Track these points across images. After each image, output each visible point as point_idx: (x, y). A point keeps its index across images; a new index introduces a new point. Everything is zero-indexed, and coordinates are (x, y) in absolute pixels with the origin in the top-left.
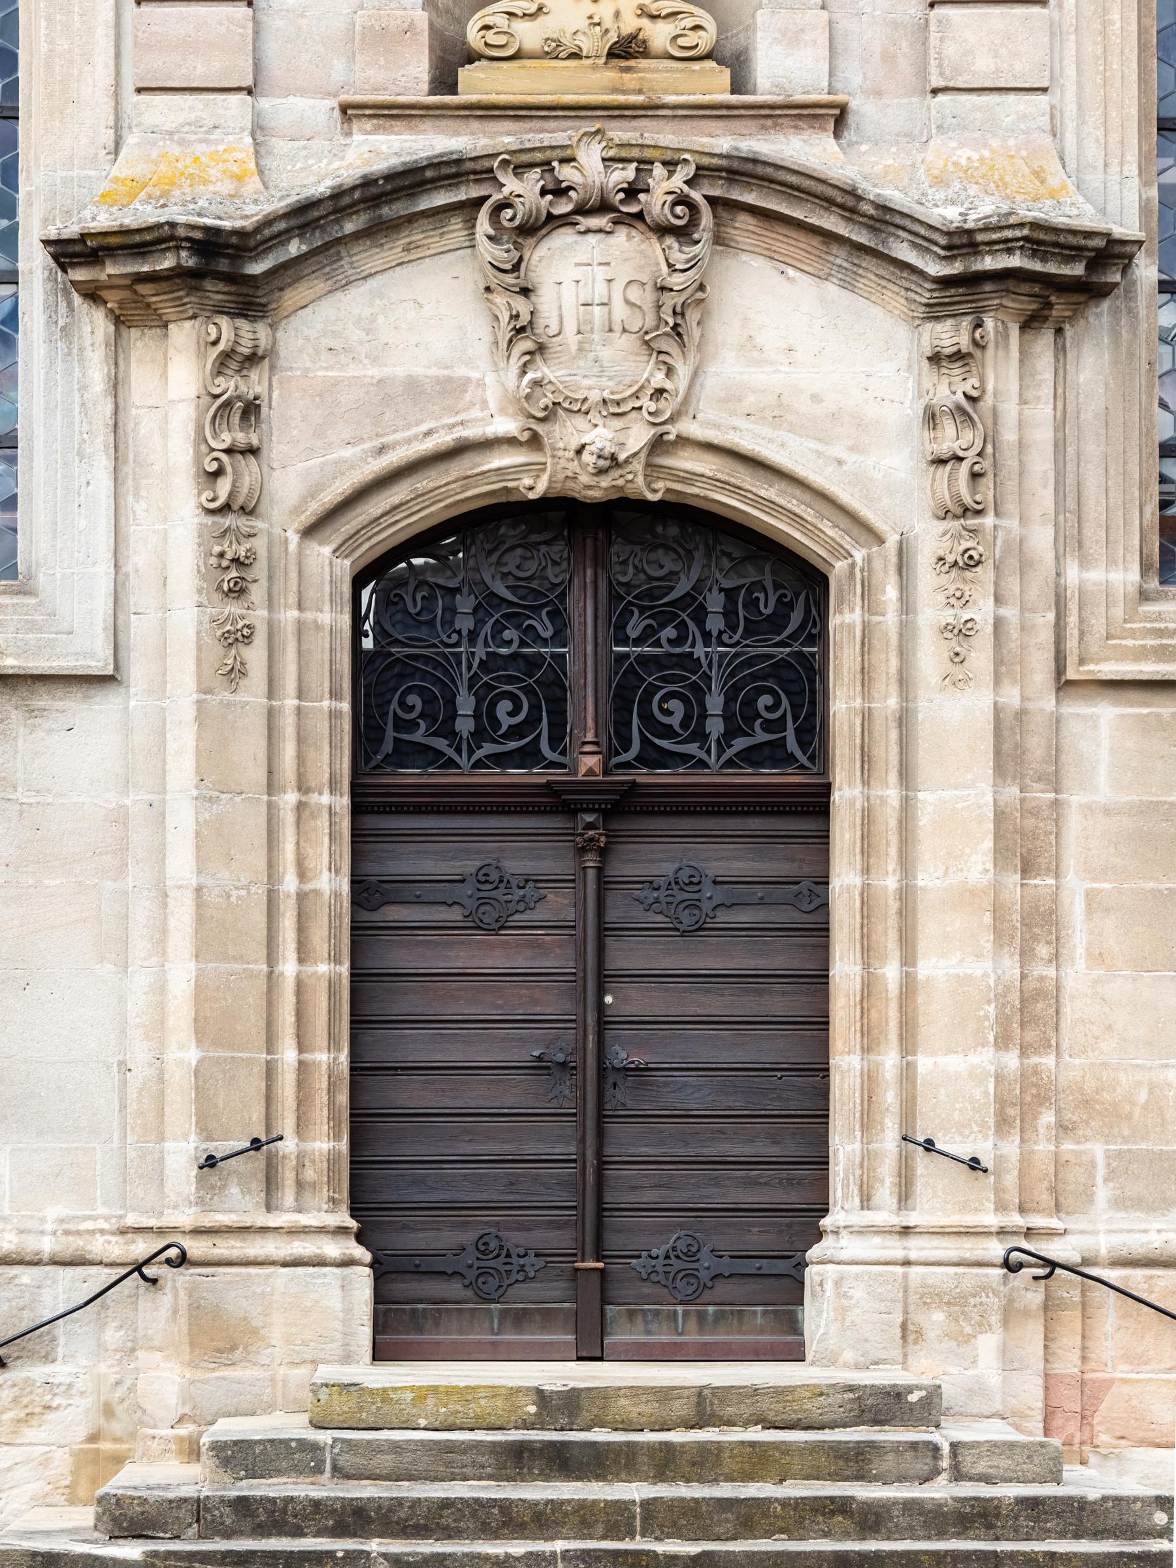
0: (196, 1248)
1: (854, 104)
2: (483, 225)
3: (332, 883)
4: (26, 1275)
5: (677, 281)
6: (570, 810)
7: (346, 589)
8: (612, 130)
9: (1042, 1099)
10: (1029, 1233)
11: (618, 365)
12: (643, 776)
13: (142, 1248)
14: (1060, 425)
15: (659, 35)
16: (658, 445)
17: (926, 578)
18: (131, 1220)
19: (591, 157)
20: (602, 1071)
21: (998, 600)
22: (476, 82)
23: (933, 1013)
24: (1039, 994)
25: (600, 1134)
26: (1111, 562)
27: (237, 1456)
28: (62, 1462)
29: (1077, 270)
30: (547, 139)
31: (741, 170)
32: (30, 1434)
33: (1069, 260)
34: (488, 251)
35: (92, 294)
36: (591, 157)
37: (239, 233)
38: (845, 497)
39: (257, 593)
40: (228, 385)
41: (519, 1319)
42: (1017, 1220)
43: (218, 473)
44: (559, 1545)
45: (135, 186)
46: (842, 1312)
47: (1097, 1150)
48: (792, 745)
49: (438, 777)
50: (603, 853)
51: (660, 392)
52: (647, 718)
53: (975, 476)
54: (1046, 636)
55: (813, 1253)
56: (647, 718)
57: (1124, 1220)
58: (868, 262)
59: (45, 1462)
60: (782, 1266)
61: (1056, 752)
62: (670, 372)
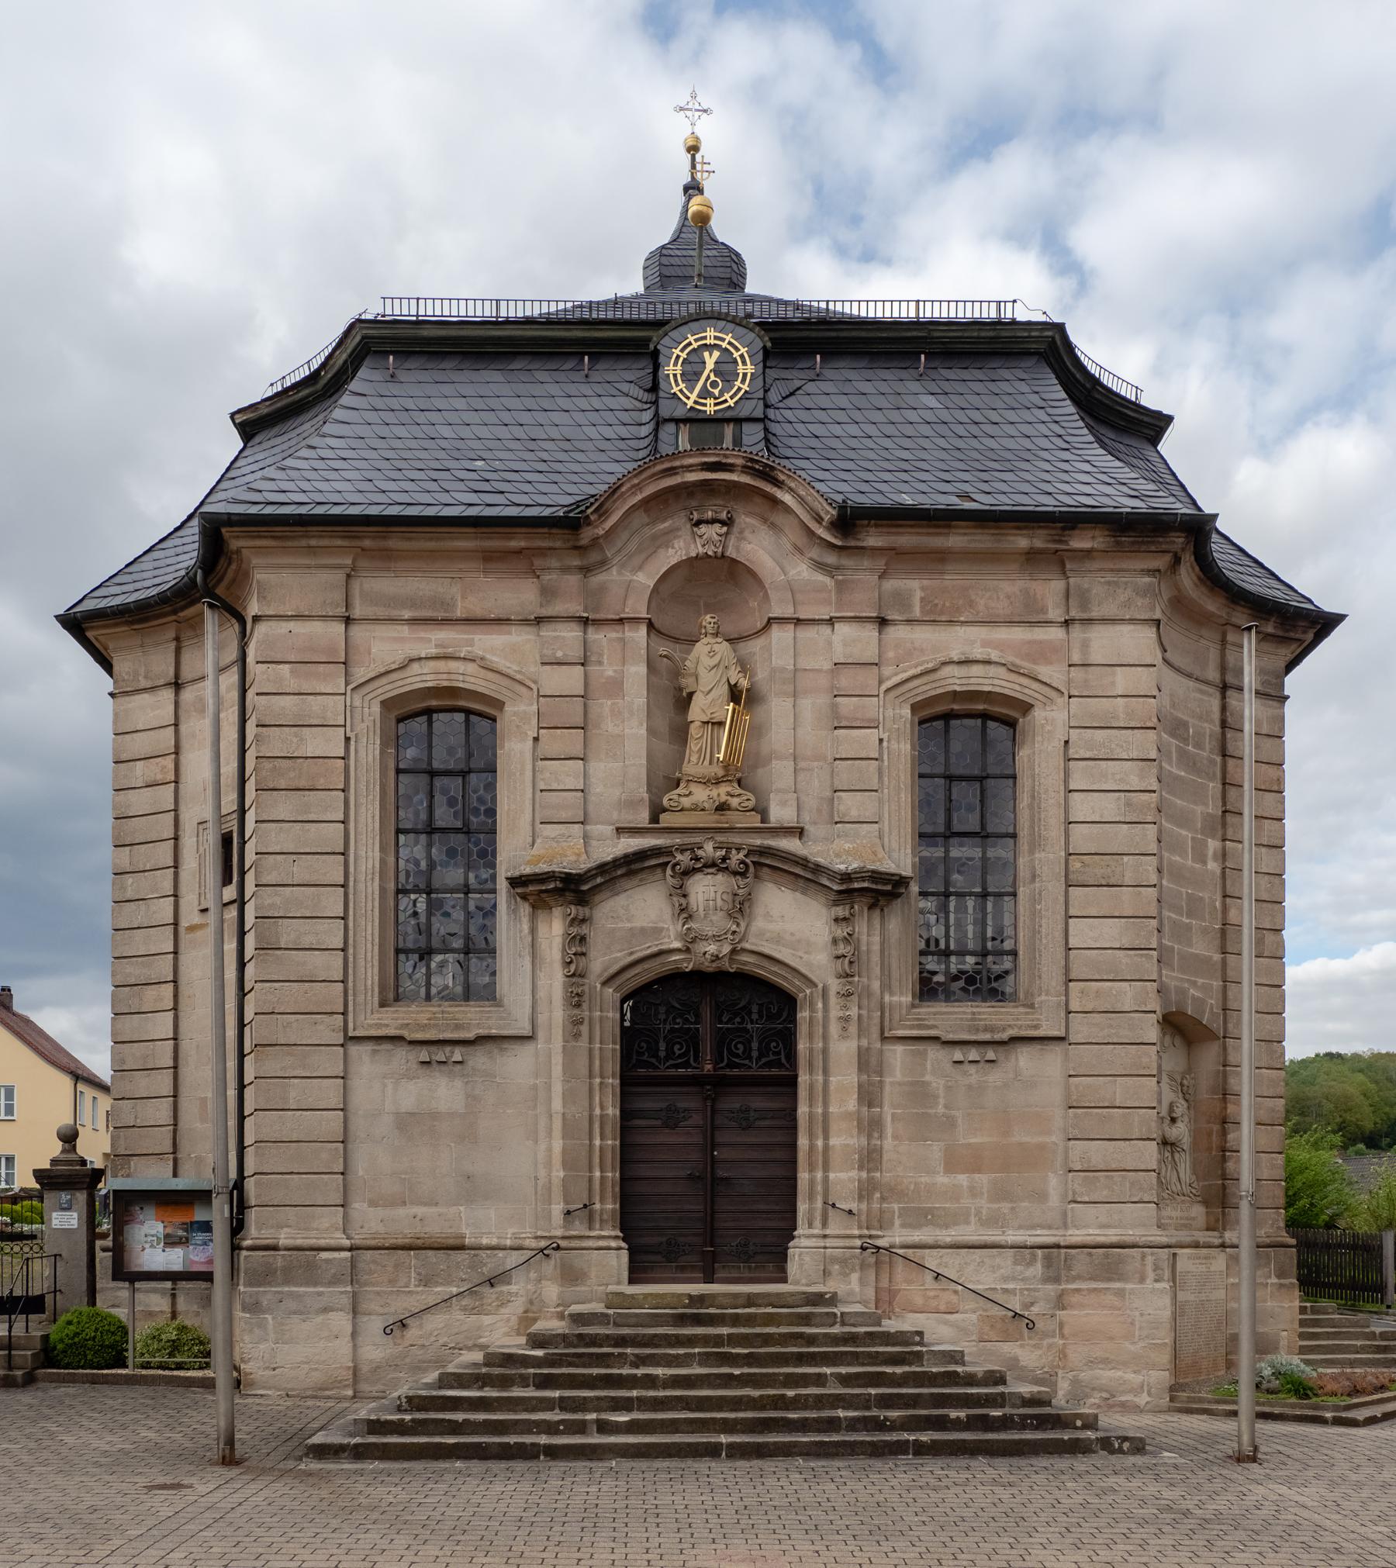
2: (669, 872)
3: (613, 1111)
4: (501, 1254)
8: (92, 628)
9: (875, 1189)
10: (870, 1237)
12: (728, 1072)
13: (543, 1244)
14: (882, 944)
15: (734, 802)
16: (734, 951)
17: (833, 1000)
18: (539, 1233)
19: (709, 847)
21: (860, 1008)
22: (666, 820)
23: (835, 1158)
24: (874, 1150)
25: (713, 1202)
26: (901, 994)
27: (578, 1319)
28: (514, 1320)
29: (889, 887)
30: (692, 840)
31: (765, 851)
32: (503, 1311)
35: (524, 897)
36: (709, 847)
39: (585, 1006)
41: (683, 1269)
42: (866, 1232)
44: (697, 1350)
45: (539, 859)
46: (801, 1265)
47: (896, 1206)
48: (783, 1060)
49: (652, 1072)
50: (714, 1100)
51: (734, 932)
53: (851, 963)
54: (877, 1021)
55: (791, 1244)
57: (905, 1232)
58: (811, 885)
59: (508, 1320)
60: (780, 1249)
61: (881, 1063)
62: (738, 925)
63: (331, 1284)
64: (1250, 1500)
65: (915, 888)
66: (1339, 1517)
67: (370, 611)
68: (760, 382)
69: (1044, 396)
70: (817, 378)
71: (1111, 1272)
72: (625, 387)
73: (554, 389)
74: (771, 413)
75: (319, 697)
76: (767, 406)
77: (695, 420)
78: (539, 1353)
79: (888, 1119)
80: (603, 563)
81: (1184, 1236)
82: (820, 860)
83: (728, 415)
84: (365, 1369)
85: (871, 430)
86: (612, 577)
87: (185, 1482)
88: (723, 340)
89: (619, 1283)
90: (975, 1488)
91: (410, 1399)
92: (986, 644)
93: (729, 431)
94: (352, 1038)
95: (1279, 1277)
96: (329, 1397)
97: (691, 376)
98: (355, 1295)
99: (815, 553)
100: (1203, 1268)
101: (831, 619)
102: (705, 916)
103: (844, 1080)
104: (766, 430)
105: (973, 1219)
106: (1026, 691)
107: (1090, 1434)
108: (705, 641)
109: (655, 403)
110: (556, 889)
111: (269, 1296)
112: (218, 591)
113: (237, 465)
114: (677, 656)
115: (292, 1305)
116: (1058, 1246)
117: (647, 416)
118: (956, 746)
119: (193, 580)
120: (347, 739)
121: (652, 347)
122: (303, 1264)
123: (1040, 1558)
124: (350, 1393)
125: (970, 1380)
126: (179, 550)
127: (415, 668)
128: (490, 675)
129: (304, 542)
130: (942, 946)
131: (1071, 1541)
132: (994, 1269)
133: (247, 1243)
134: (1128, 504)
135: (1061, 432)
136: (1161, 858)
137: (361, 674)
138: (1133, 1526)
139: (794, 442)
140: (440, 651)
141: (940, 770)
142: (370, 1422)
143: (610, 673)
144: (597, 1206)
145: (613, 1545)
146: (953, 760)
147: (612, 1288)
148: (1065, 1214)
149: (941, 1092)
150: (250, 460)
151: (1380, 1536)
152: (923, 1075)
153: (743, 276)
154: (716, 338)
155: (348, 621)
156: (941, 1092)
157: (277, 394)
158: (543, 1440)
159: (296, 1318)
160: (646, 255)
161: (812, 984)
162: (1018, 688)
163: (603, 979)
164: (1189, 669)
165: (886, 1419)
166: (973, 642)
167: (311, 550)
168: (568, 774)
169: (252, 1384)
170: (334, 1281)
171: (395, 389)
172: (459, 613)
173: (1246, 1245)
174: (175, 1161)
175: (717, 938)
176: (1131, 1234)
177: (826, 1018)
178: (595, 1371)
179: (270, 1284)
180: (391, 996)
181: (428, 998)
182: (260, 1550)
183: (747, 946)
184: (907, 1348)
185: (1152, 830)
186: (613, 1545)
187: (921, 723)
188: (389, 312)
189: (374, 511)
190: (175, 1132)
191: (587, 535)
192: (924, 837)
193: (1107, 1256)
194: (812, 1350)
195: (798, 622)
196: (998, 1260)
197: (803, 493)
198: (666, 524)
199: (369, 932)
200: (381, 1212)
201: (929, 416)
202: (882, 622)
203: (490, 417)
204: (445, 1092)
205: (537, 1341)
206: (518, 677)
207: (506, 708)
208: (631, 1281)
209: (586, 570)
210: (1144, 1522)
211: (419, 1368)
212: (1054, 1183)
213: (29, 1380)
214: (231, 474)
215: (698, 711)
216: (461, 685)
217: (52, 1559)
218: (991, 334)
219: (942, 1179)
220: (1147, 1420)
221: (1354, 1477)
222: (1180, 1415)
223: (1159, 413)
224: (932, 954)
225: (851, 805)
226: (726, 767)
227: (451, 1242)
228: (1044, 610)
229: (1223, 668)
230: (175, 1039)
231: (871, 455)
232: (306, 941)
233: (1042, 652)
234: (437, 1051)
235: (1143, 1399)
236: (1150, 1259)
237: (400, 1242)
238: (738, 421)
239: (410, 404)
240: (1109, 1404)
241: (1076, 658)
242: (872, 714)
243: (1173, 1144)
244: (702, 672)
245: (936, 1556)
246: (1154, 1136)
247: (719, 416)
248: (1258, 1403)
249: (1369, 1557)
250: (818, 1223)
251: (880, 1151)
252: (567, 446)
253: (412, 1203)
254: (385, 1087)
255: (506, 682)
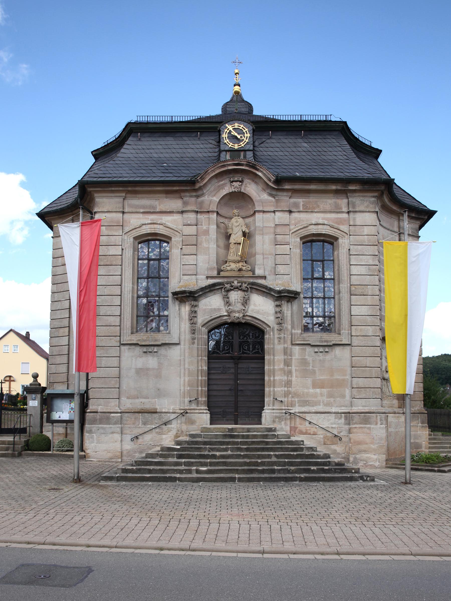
0: (188, 411)
1: (267, 276)
2: (223, 290)
3: (205, 368)
4: (169, 415)
5: (246, 297)
6: (234, 359)
7: (207, 333)
8: (47, 217)
9: (290, 394)
10: (288, 409)
11: (239, 307)
12: (242, 355)
13: (182, 411)
14: (292, 313)
15: (244, 268)
16: (244, 316)
17: (276, 332)
18: (181, 408)
19: (236, 282)
20: (237, 390)
21: (284, 334)
22: (222, 274)
24: (289, 381)
25: (237, 398)
26: (298, 330)
27: (192, 436)
29: (293, 295)
30: (230, 280)
31: (253, 284)
32: (169, 433)
33: (292, 294)
34: (224, 293)
35: (177, 299)
36: (236, 282)
37: (194, 291)
38: (266, 322)
39: (196, 333)
40: (193, 309)
41: (227, 420)
42: (287, 408)
43: (191, 320)
44: (230, 446)
45: (182, 286)
46: (266, 419)
47: (296, 399)
48: (260, 351)
49: (218, 355)
50: (237, 364)
51: (244, 310)
52: (243, 349)
53: (281, 319)
54: (290, 338)
55: (263, 412)
56: (243, 349)
57: (299, 408)
59: (171, 437)
60: (259, 414)
61: (291, 352)
62: (245, 307)
63: (114, 424)
64: (407, 496)
65: (302, 296)
66: (435, 502)
67: (130, 210)
68: (252, 139)
69: (341, 143)
70: (271, 138)
71: (366, 421)
72: (211, 141)
73: (189, 142)
74: (256, 149)
75: (114, 237)
76: (254, 146)
77: (232, 151)
78: (179, 447)
79: (294, 371)
80: (203, 195)
81: (390, 410)
82: (271, 287)
83: (242, 149)
84: (125, 453)
85: (287, 154)
86: (206, 198)
87: (61, 488)
88: (240, 127)
89: (207, 424)
90: (318, 491)
91: (136, 462)
92: (323, 219)
93: (242, 154)
94: (122, 344)
95: (422, 423)
96: (113, 462)
97: (238, 140)
98: (122, 428)
99: (268, 191)
100: (397, 420)
101: (274, 211)
102: (235, 305)
103: (279, 357)
104: (254, 153)
105: (321, 404)
106: (336, 233)
107: (357, 475)
108: (235, 218)
109: (219, 146)
110: (187, 296)
111: (95, 428)
112: (84, 205)
113: (93, 167)
114: (226, 223)
115: (102, 431)
116: (349, 413)
117: (217, 150)
118: (314, 251)
119: (77, 201)
120: (123, 249)
121: (218, 129)
122: (106, 418)
123: (334, 515)
124: (120, 460)
125: (318, 457)
126: (74, 193)
127: (144, 227)
128: (167, 229)
129: (110, 189)
130: (311, 314)
131: (346, 510)
132: (328, 420)
133: (88, 411)
134: (366, 176)
135: (346, 154)
136: (380, 287)
137: (127, 229)
138: (367, 505)
139: (263, 157)
140: (152, 222)
141: (310, 258)
142: (122, 469)
143: (205, 228)
144: (200, 399)
145: (194, 510)
146: (314, 255)
147: (204, 426)
148: (351, 402)
149: (311, 362)
150: (97, 165)
151: (447, 508)
152: (305, 356)
153: (252, 111)
154: (238, 126)
155: (123, 213)
156: (311, 362)
157: (105, 146)
158: (178, 476)
159: (103, 435)
160: (222, 105)
161: (269, 327)
162: (333, 232)
163: (202, 325)
164: (388, 227)
165: (290, 469)
166: (319, 218)
167: (113, 192)
168: (191, 260)
169: (89, 457)
170: (115, 423)
171: (140, 143)
172: (158, 210)
173: (408, 411)
174: (68, 384)
175: (239, 312)
176: (373, 409)
177: (274, 338)
178: (196, 453)
179: (95, 424)
180: (135, 330)
181: (147, 331)
182: (79, 510)
183: (248, 314)
184: (297, 446)
185: (377, 277)
186: (194, 510)
187: (303, 243)
188: (139, 120)
189: (132, 179)
190: (68, 375)
191: (198, 185)
192: (305, 280)
193: (365, 416)
194: (267, 446)
195: (264, 212)
196: (330, 417)
197: (265, 172)
198: (222, 182)
199: (128, 310)
200: (130, 401)
201: (305, 149)
202: (290, 212)
203: (169, 151)
204: (151, 362)
205: (178, 443)
206: (176, 229)
207: (173, 239)
208: (211, 424)
209: (198, 197)
210: (371, 504)
211: (141, 452)
212: (347, 392)
213: (20, 455)
214: (90, 170)
215: (232, 240)
216: (158, 232)
217: (12, 511)
218: (324, 125)
219: (311, 391)
220: (378, 471)
221: (442, 489)
222: (389, 469)
223: (377, 149)
224: (308, 317)
225: (281, 269)
226: (241, 257)
227: (153, 411)
228: (341, 208)
229: (399, 227)
230: (69, 345)
231: (287, 161)
232: (108, 313)
233: (340, 221)
234: (149, 348)
235: (377, 464)
236: (379, 417)
237: (136, 410)
238: (245, 151)
239: (144, 147)
240: (366, 465)
241: (352, 223)
242: (287, 240)
243: (387, 380)
244: (234, 228)
245: (300, 515)
246: (380, 376)
247: (239, 149)
248: (412, 465)
249: (443, 515)
250: (271, 405)
251: (291, 381)
252: (192, 159)
253: (140, 398)
254: (132, 360)
255: (173, 231)
